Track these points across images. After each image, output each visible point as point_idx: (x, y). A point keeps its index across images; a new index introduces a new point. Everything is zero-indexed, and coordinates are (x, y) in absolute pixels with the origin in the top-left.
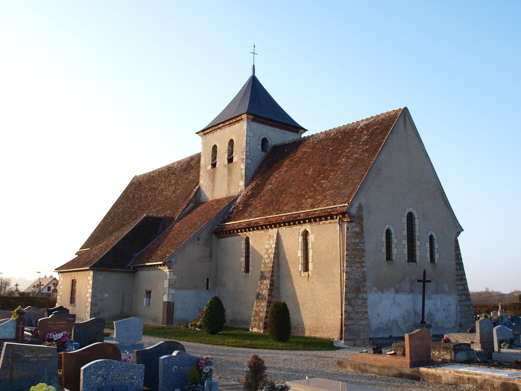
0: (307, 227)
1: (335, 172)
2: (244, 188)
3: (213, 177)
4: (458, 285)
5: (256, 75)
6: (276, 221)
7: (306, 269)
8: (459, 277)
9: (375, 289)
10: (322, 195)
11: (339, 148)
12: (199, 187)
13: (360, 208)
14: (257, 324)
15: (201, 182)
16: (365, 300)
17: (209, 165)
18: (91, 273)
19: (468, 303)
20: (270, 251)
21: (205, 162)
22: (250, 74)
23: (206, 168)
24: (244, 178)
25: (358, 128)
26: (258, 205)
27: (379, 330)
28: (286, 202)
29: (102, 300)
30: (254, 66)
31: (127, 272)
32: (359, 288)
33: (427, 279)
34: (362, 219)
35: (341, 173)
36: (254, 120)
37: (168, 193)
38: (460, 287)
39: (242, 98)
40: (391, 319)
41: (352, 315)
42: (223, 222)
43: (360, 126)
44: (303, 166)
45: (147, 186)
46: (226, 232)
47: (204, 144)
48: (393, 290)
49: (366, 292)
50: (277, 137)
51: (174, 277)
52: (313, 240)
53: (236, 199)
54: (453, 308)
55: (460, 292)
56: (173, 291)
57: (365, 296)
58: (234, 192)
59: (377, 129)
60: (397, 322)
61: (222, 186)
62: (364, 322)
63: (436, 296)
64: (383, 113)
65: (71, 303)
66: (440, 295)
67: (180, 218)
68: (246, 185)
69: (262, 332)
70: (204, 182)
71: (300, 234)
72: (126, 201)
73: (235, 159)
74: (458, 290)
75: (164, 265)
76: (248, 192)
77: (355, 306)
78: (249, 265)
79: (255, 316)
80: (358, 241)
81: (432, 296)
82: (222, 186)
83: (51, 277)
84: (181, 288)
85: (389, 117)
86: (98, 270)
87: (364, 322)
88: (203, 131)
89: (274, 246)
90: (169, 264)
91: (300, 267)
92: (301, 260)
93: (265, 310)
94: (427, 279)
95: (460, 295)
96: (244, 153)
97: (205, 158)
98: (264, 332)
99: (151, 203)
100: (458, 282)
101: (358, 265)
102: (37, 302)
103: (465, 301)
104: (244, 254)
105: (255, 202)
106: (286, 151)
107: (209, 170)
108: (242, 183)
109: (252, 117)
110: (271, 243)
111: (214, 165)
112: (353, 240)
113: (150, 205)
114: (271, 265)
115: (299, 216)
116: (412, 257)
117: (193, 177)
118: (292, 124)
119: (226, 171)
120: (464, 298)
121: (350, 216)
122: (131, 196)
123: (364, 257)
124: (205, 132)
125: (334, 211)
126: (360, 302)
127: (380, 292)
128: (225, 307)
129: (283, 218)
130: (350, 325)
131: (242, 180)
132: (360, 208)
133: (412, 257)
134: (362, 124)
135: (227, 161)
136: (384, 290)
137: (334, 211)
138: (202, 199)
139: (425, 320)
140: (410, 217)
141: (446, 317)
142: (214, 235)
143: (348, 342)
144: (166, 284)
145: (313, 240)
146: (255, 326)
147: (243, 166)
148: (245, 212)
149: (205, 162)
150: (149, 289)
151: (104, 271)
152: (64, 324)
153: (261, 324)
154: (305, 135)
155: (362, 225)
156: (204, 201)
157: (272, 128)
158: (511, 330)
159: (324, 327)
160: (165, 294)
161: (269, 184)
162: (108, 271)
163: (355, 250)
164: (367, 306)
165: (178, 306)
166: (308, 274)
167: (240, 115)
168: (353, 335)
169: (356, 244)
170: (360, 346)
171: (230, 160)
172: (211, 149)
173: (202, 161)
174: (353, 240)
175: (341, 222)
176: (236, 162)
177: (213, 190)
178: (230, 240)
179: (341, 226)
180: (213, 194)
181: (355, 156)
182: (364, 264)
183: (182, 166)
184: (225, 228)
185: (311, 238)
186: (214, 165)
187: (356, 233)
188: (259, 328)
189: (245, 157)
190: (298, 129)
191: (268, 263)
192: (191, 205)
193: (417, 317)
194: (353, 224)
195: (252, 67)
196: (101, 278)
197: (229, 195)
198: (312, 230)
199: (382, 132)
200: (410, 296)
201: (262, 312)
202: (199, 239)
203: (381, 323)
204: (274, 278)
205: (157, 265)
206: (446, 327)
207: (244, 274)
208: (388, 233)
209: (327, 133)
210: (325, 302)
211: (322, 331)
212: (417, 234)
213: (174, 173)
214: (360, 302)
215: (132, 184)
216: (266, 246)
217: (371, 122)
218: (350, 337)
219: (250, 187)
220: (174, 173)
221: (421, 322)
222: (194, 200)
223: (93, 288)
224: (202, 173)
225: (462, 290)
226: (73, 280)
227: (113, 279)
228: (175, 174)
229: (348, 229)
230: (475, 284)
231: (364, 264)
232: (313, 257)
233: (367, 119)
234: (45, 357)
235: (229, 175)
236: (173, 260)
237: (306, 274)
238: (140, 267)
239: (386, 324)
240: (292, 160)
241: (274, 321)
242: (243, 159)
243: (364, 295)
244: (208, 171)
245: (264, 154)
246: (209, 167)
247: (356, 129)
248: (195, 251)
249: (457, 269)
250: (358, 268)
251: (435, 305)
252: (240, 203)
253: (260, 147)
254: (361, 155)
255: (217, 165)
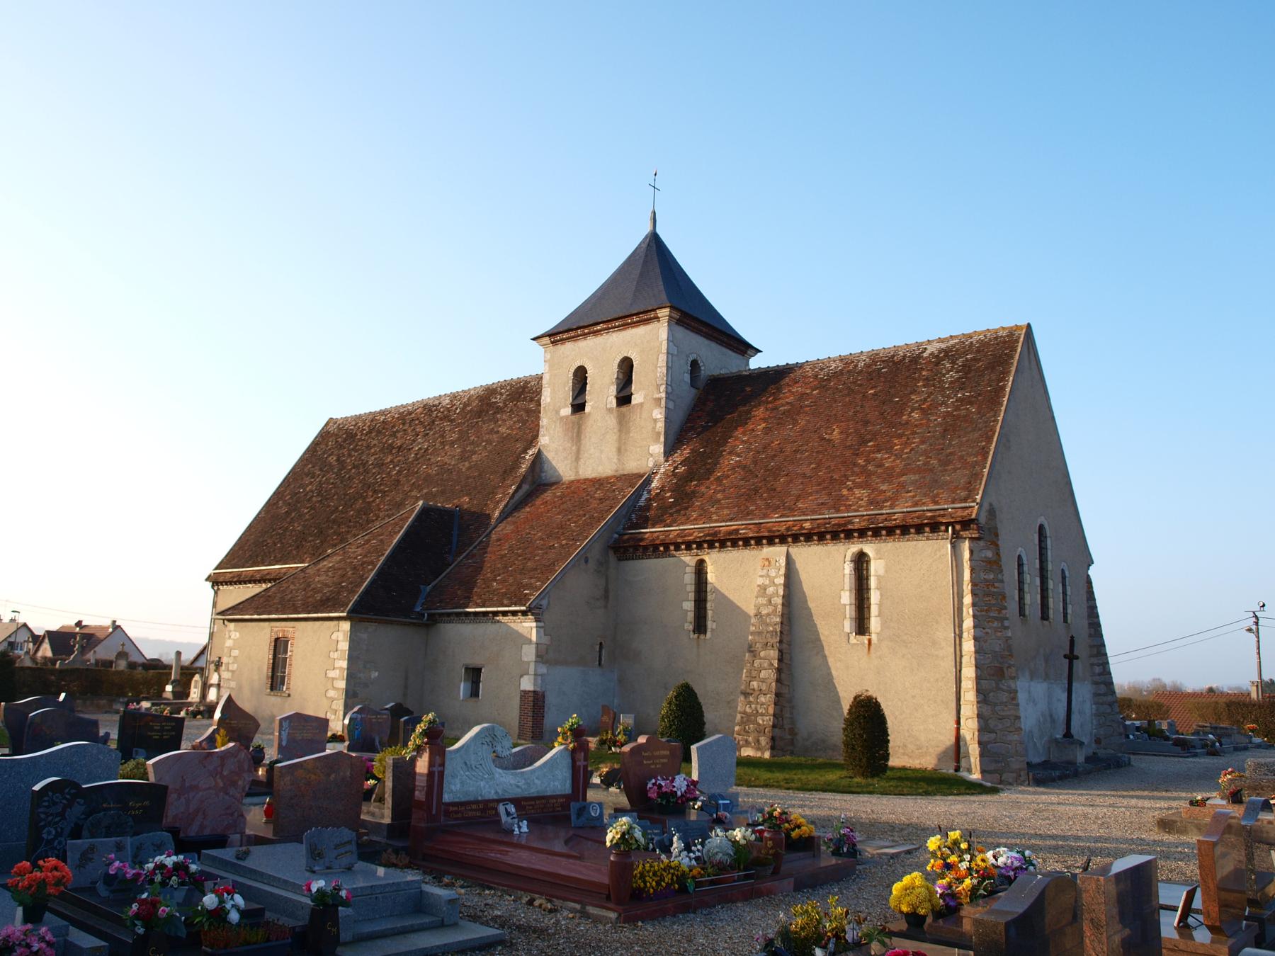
0: (869, 548)
1: (904, 439)
2: (662, 459)
3: (576, 433)
4: (1092, 665)
5: (658, 231)
6: (788, 529)
7: (861, 626)
8: (1095, 651)
10: (890, 483)
11: (892, 391)
12: (539, 455)
13: (992, 512)
14: (750, 739)
15: (544, 440)
16: (1013, 693)
17: (566, 406)
18: (346, 626)
19: (1110, 698)
20: (771, 590)
21: (555, 399)
22: (647, 229)
23: (558, 412)
24: (662, 439)
25: (925, 355)
26: (719, 496)
28: (794, 492)
29: (366, 685)
30: (654, 213)
31: (414, 624)
32: (1001, 670)
34: (997, 535)
35: (923, 442)
36: (679, 322)
37: (446, 459)
38: (1097, 670)
39: (641, 275)
41: (992, 723)
42: (629, 527)
43: (928, 352)
44: (808, 422)
45: (374, 442)
46: (646, 548)
47: (551, 363)
49: (1013, 678)
50: (716, 361)
51: (546, 640)
52: (881, 572)
53: (648, 481)
55: (1097, 678)
56: (543, 669)
57: (1013, 686)
58: (634, 464)
59: (974, 359)
61: (601, 452)
62: (1016, 737)
64: (1005, 325)
65: (272, 689)
67: (504, 516)
68: (668, 453)
69: (767, 755)
70: (551, 441)
71: (848, 558)
72: (321, 470)
73: (636, 399)
74: (1093, 674)
75: (524, 613)
76: (676, 468)
77: (995, 705)
78: (705, 617)
79: (742, 723)
80: (992, 576)
82: (601, 452)
83: (13, 620)
84: (557, 663)
85: (996, 338)
86: (361, 620)
87: (1016, 737)
88: (550, 334)
89: (781, 580)
90: (537, 611)
91: (848, 626)
92: (850, 612)
93: (771, 711)
95: (1096, 683)
96: (663, 388)
97: (553, 392)
98: (772, 755)
99: (403, 480)
100: (1094, 660)
101: (995, 624)
102: (82, 676)
103: (1105, 695)
104: (692, 596)
105: (708, 489)
106: (748, 389)
107: (567, 417)
108: (658, 449)
109: (676, 315)
110: (773, 573)
111: (578, 407)
112: (982, 576)
113: (398, 481)
114: (778, 620)
115: (851, 523)
117: (510, 428)
119: (612, 421)
120: (1103, 689)
121: (979, 529)
122: (333, 459)
123: (1005, 608)
124: (556, 336)
125: (943, 516)
126: (1004, 697)
128: (701, 700)
129: (807, 525)
130: (989, 742)
131: (657, 441)
132: (992, 512)
134: (931, 349)
135: (614, 401)
137: (943, 516)
138: (547, 476)
139: (1073, 731)
142: (611, 553)
143: (988, 776)
144: (529, 654)
145: (881, 572)
146: (747, 744)
147: (659, 414)
148: (686, 508)
149: (555, 399)
150: (475, 661)
151: (369, 621)
152: (664, 757)
153: (764, 741)
154: (755, 363)
155: (997, 545)
156: (553, 480)
157: (706, 342)
159: (911, 747)
160: (527, 674)
161: (730, 453)
162: (380, 622)
163: (988, 595)
164: (1018, 705)
165: (551, 700)
166: (870, 641)
167: (654, 310)
168: (997, 762)
169: (989, 583)
170: (1011, 784)
171: (624, 399)
172: (571, 375)
173: (546, 397)
174: (982, 576)
175: (957, 537)
176: (641, 405)
177: (577, 459)
178: (652, 565)
179: (954, 546)
180: (576, 468)
181: (943, 409)
182: (1006, 623)
183: (466, 405)
184: (642, 540)
185: (876, 568)
186: (578, 407)
187: (989, 562)
188: (758, 749)
189: (663, 395)
190: (745, 349)
191: (768, 615)
192: (525, 487)
194: (982, 543)
195: (650, 215)
196: (365, 636)
197: (621, 472)
198: (878, 551)
199: (993, 368)
200: (1045, 685)
201: (762, 715)
202: (586, 562)
204: (784, 646)
205: (496, 614)
207: (854, 639)
209: (848, 363)
210: (913, 697)
211: (904, 754)
213: (446, 418)
214: (1004, 697)
215: (324, 436)
216: (760, 581)
217: (953, 346)
218: (993, 767)
219: (678, 457)
220: (446, 418)
221: (1065, 736)
222: (530, 478)
223: (352, 659)
224: (544, 421)
225: (1100, 674)
226: (277, 640)
227: (387, 636)
228: (452, 421)
229: (971, 552)
230: (1131, 667)
231: (1006, 623)
232: (880, 605)
233: (940, 340)
235: (620, 431)
236: (544, 602)
237: (865, 639)
238: (449, 615)
240: (775, 408)
241: (861, 736)
242: (660, 399)
243: (1012, 683)
244: (562, 418)
245: (694, 391)
246: (567, 411)
247: (919, 356)
248: (582, 584)
249: (1090, 636)
250: (996, 630)
252: (662, 489)
253: (687, 377)
254: (957, 408)
255: (588, 409)
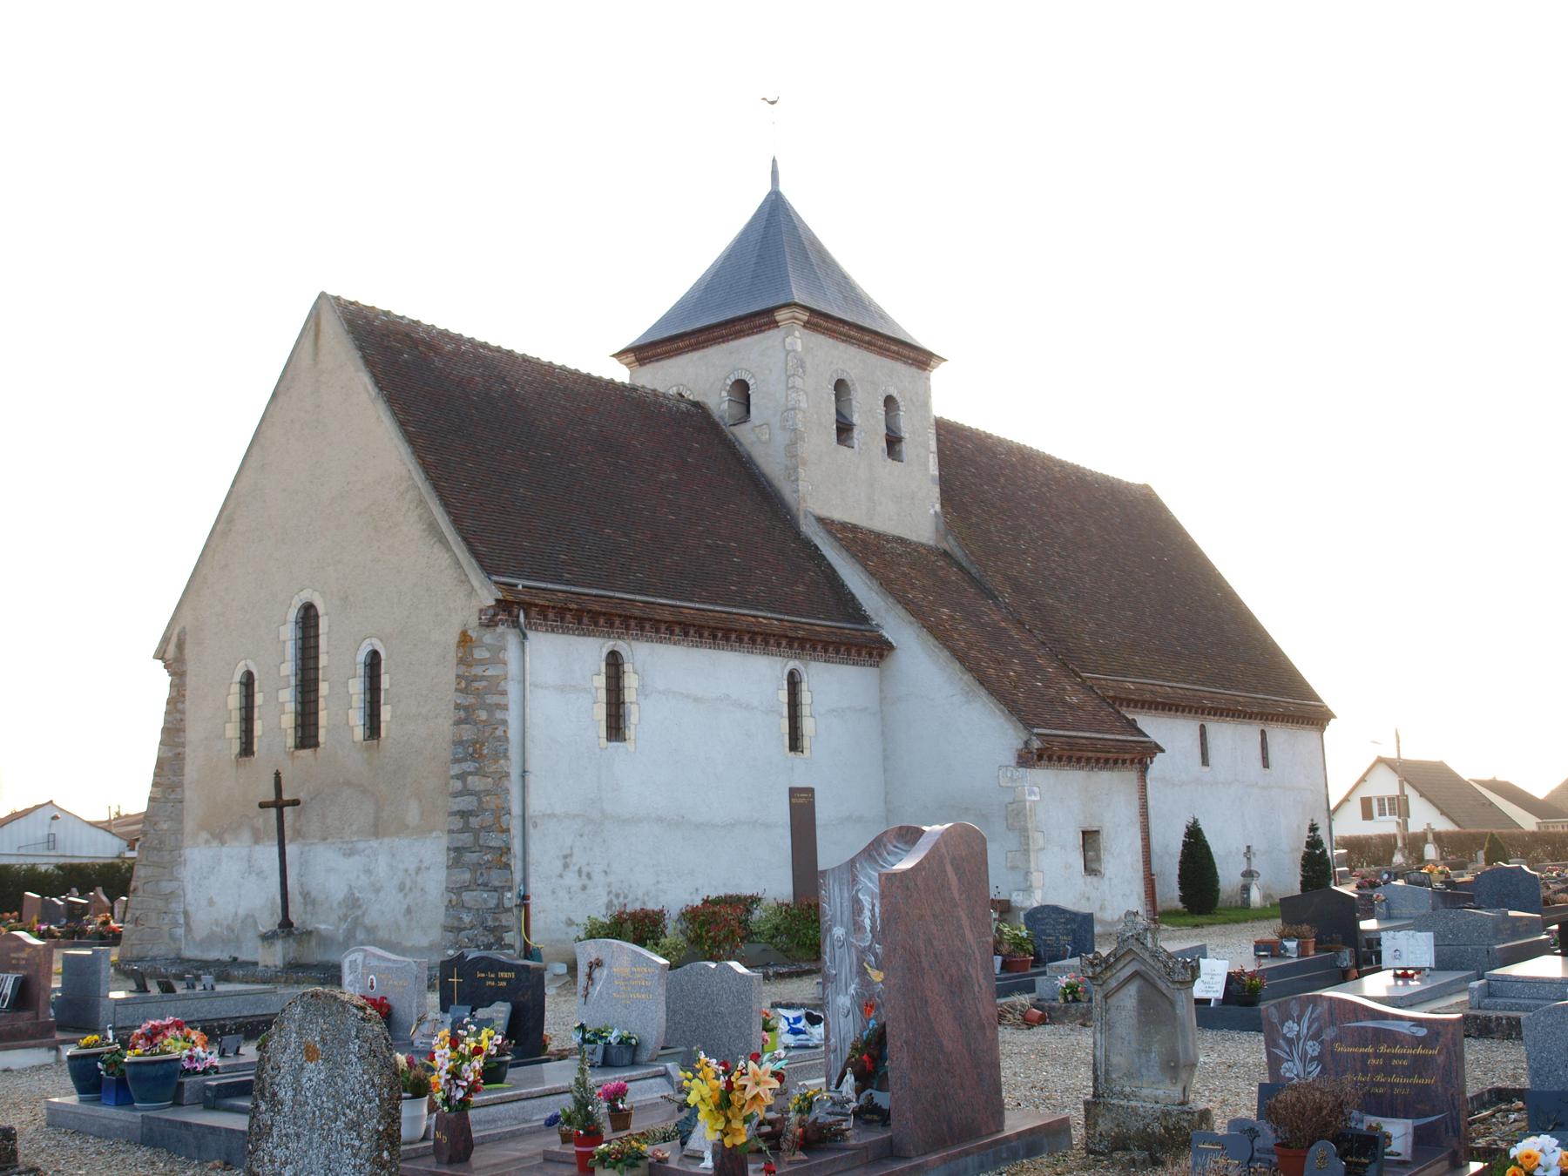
9: (205, 835)
27: (210, 940)
33: (286, 797)
40: (241, 913)
48: (246, 836)
54: (435, 882)
60: (255, 923)
63: (374, 843)
66: (386, 840)
81: (361, 845)
94: (286, 797)
116: (307, 734)
118: (867, 324)
127: (215, 844)
133: (307, 734)
136: (226, 836)
140: (308, 618)
141: (409, 911)
158: (663, 961)
193: (309, 908)
203: (217, 923)
206: (409, 944)
208: (248, 682)
212: (323, 660)
234: (1404, 1085)
239: (229, 927)
251: (368, 872)
